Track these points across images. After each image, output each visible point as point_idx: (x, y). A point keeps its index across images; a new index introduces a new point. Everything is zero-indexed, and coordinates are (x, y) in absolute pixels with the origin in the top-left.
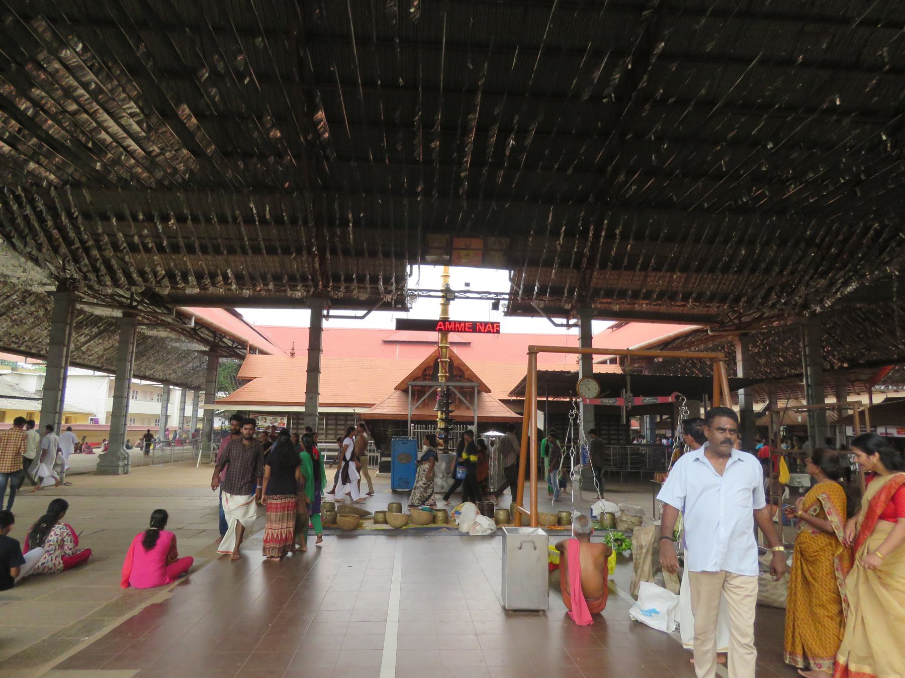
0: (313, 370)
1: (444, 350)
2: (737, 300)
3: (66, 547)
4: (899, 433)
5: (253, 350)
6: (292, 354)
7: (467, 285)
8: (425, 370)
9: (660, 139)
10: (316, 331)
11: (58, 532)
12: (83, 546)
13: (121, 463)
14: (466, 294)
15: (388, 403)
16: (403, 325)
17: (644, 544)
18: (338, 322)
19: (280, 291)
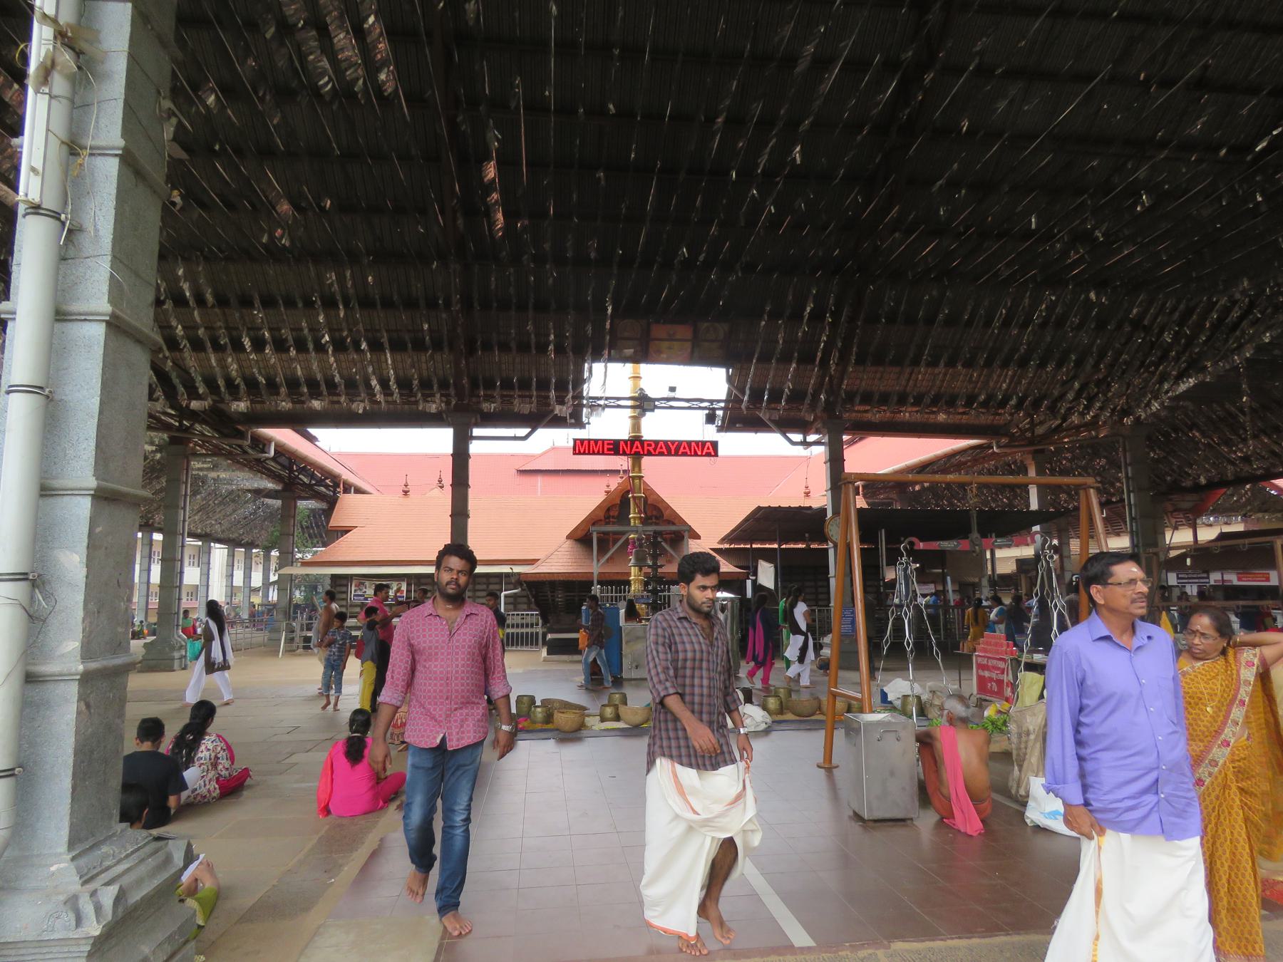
0: (460, 514)
1: (637, 481)
2: (1036, 405)
3: (220, 767)
4: (1239, 579)
5: (348, 488)
6: (406, 493)
7: (673, 389)
8: (608, 510)
9: (953, 185)
10: (461, 458)
11: (210, 746)
12: (239, 765)
13: (176, 655)
14: (669, 402)
15: (557, 558)
16: (583, 447)
17: (1031, 728)
18: (493, 445)
19: (409, 403)
